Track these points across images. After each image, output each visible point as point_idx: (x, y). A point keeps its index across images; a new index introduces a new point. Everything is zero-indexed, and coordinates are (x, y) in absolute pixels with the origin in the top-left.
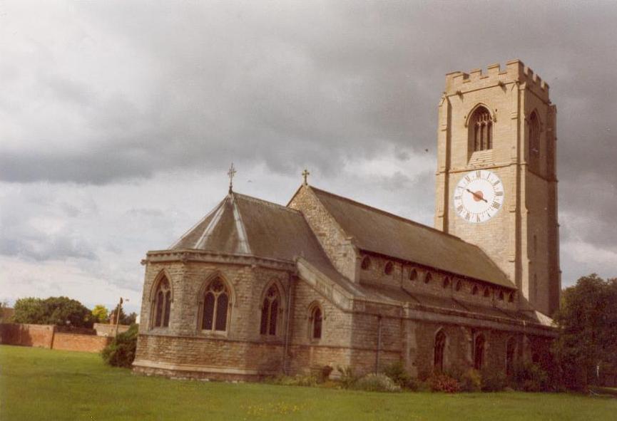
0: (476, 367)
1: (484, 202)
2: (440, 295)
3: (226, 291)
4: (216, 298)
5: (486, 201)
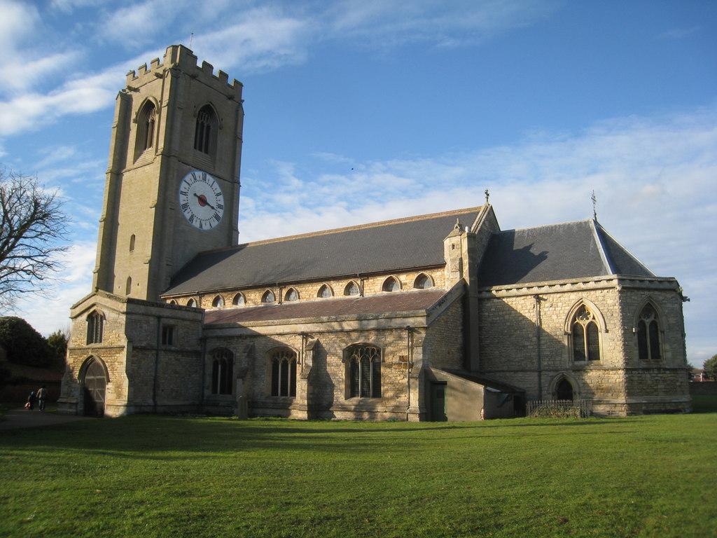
0: (204, 329)
3: (594, 318)
4: (648, 325)
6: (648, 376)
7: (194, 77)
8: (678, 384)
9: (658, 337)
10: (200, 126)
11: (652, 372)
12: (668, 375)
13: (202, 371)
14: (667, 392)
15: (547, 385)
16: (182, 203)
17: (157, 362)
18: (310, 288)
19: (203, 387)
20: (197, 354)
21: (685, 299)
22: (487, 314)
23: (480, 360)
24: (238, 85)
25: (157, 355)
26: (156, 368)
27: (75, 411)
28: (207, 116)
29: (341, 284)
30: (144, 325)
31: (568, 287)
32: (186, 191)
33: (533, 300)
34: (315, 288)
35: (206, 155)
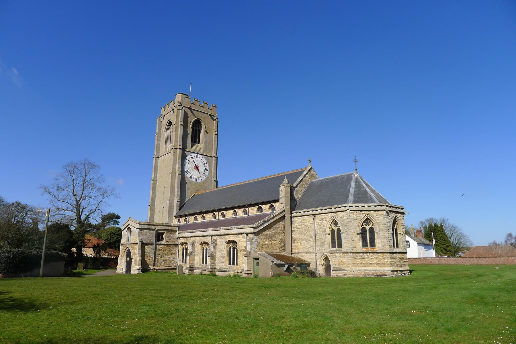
3: (339, 226)
4: (368, 230)
6: (366, 256)
8: (385, 261)
9: (374, 236)
11: (368, 254)
14: (378, 265)
15: (319, 260)
28: (198, 125)
31: (328, 210)
34: (231, 211)
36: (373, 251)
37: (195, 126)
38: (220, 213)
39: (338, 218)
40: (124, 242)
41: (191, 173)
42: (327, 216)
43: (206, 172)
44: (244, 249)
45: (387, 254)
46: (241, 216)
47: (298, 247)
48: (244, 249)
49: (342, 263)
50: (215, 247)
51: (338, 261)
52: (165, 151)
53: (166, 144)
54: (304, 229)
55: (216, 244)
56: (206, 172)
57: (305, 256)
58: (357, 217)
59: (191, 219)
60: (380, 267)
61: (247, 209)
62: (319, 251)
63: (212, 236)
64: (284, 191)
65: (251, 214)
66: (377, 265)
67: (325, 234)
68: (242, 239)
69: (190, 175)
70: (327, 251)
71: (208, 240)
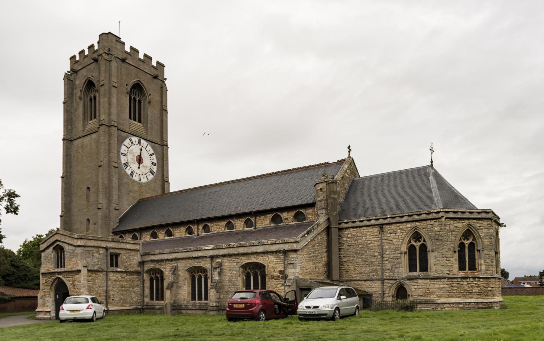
0: (141, 255)
1: (138, 166)
2: (4, 293)
3: (424, 241)
4: (467, 246)
5: (139, 168)
6: (465, 283)
7: (123, 60)
8: (489, 289)
10: (132, 101)
11: (468, 280)
12: (482, 283)
13: (142, 286)
14: (480, 295)
15: (388, 290)
16: (123, 162)
17: (107, 280)
18: (220, 223)
19: (144, 296)
20: (138, 273)
21: (500, 225)
22: (345, 239)
23: (340, 272)
24: (161, 66)
25: (107, 275)
26: (107, 285)
27: (49, 317)
28: (137, 92)
29: (241, 220)
30: (95, 254)
32: (126, 153)
33: (376, 230)
34: (223, 223)
35: (139, 124)
36: (474, 276)
37: (134, 92)
38: (201, 227)
39: (423, 229)
40: (48, 270)
41: (132, 168)
42: (404, 227)
43: (153, 168)
44: (279, 275)
45: (491, 280)
46: (242, 229)
47: (349, 272)
48: (279, 275)
49: (429, 293)
50: (220, 274)
51: (422, 290)
52: (83, 131)
53: (85, 119)
54: (361, 246)
55: (221, 269)
56: (153, 168)
57: (362, 285)
58: (455, 228)
59: (144, 236)
60: (482, 297)
61: (253, 219)
62: (388, 277)
63: (212, 257)
64: (324, 190)
65: (260, 227)
66: (478, 294)
67: (399, 252)
68: (275, 261)
69: (130, 171)
70: (404, 277)
71: (205, 264)
